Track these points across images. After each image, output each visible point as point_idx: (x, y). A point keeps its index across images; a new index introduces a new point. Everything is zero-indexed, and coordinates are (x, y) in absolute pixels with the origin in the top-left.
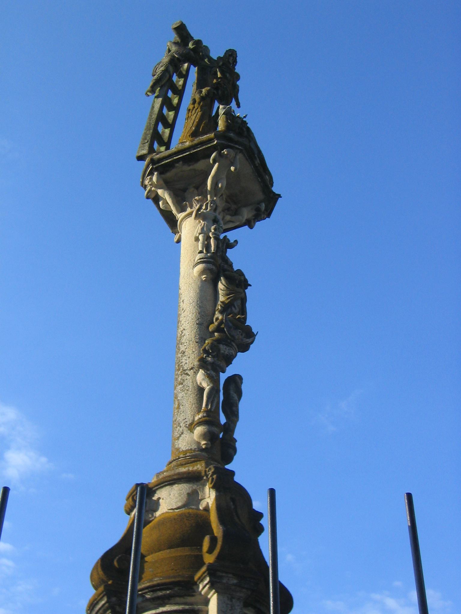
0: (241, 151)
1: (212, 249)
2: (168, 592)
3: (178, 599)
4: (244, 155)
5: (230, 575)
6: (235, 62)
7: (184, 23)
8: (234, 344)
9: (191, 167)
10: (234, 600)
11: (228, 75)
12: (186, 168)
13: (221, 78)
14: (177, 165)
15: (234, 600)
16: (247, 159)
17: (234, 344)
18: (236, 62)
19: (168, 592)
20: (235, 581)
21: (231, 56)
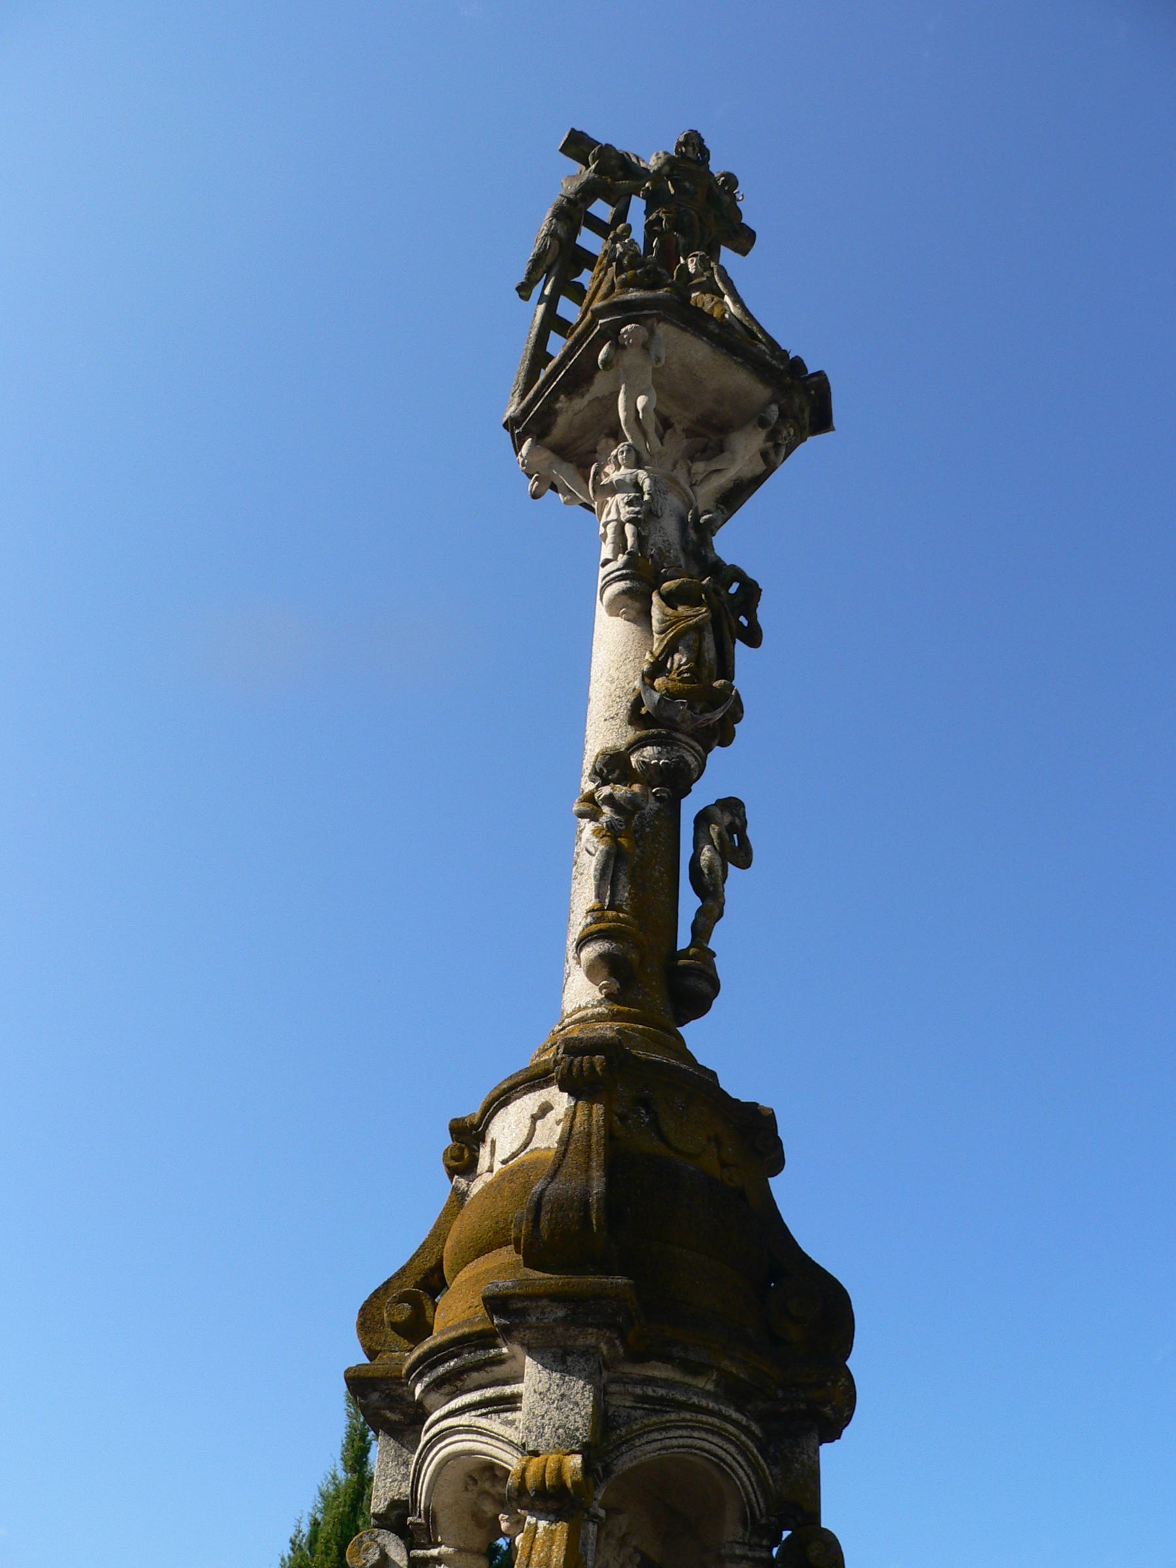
0: (660, 319)
1: (630, 543)
2: (452, 1364)
3: (476, 1377)
4: (672, 323)
5: (545, 1302)
6: (705, 152)
7: (578, 129)
8: (679, 736)
9: (588, 397)
10: (569, 1359)
11: (687, 184)
12: (580, 403)
13: (697, 204)
14: (558, 406)
15: (569, 1359)
16: (684, 330)
17: (679, 736)
18: (708, 152)
19: (452, 1364)
20: (561, 1313)
21: (694, 148)
